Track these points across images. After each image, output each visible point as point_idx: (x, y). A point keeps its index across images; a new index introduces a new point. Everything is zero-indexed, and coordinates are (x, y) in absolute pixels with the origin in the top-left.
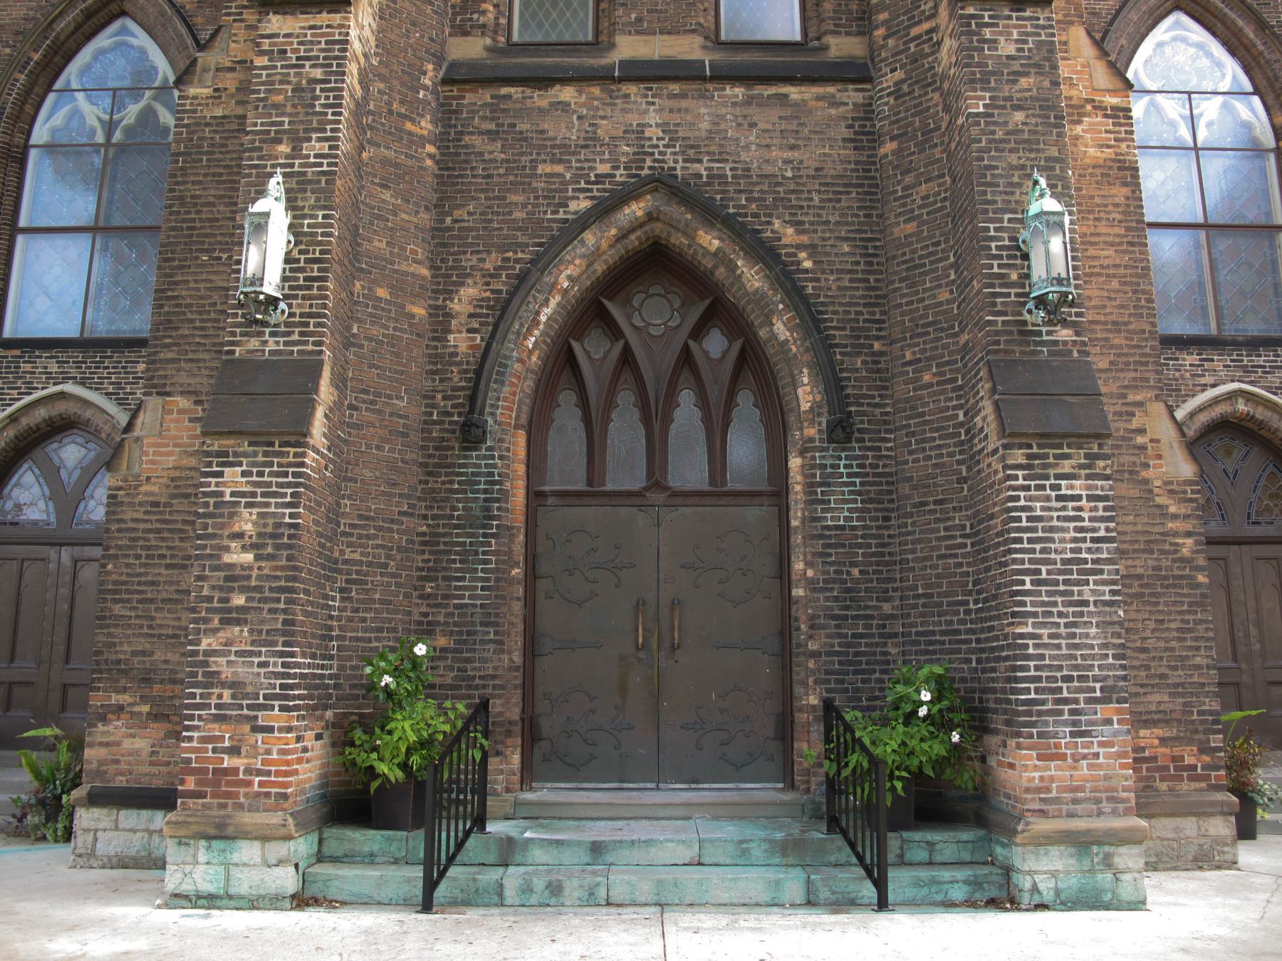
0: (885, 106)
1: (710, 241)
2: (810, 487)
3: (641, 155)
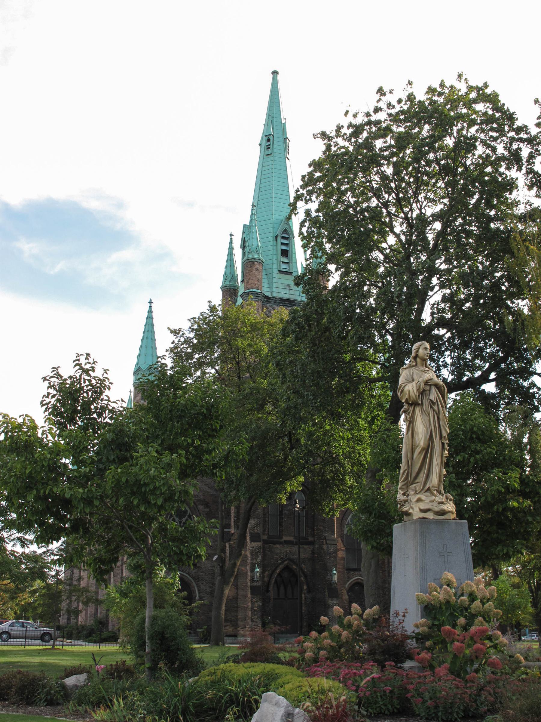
0: (316, 550)
1: (294, 567)
2: (305, 599)
3: (287, 555)
